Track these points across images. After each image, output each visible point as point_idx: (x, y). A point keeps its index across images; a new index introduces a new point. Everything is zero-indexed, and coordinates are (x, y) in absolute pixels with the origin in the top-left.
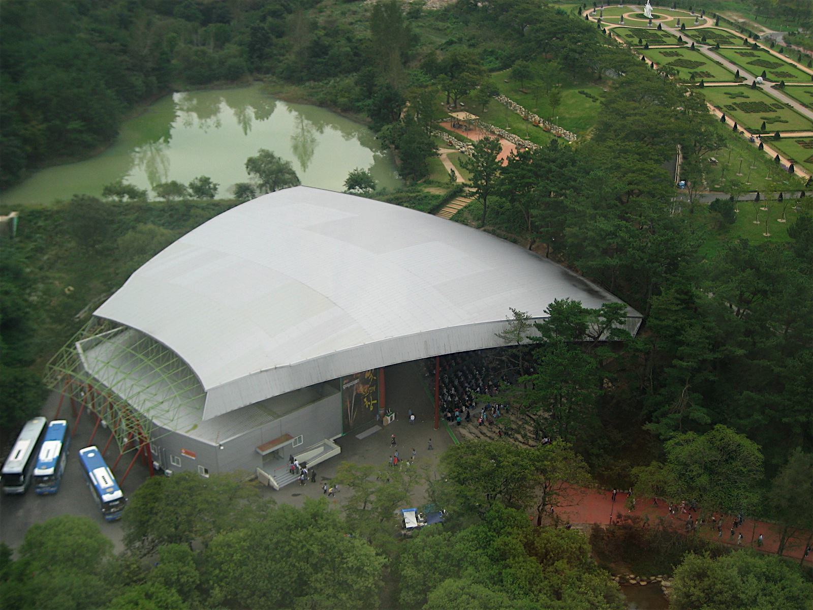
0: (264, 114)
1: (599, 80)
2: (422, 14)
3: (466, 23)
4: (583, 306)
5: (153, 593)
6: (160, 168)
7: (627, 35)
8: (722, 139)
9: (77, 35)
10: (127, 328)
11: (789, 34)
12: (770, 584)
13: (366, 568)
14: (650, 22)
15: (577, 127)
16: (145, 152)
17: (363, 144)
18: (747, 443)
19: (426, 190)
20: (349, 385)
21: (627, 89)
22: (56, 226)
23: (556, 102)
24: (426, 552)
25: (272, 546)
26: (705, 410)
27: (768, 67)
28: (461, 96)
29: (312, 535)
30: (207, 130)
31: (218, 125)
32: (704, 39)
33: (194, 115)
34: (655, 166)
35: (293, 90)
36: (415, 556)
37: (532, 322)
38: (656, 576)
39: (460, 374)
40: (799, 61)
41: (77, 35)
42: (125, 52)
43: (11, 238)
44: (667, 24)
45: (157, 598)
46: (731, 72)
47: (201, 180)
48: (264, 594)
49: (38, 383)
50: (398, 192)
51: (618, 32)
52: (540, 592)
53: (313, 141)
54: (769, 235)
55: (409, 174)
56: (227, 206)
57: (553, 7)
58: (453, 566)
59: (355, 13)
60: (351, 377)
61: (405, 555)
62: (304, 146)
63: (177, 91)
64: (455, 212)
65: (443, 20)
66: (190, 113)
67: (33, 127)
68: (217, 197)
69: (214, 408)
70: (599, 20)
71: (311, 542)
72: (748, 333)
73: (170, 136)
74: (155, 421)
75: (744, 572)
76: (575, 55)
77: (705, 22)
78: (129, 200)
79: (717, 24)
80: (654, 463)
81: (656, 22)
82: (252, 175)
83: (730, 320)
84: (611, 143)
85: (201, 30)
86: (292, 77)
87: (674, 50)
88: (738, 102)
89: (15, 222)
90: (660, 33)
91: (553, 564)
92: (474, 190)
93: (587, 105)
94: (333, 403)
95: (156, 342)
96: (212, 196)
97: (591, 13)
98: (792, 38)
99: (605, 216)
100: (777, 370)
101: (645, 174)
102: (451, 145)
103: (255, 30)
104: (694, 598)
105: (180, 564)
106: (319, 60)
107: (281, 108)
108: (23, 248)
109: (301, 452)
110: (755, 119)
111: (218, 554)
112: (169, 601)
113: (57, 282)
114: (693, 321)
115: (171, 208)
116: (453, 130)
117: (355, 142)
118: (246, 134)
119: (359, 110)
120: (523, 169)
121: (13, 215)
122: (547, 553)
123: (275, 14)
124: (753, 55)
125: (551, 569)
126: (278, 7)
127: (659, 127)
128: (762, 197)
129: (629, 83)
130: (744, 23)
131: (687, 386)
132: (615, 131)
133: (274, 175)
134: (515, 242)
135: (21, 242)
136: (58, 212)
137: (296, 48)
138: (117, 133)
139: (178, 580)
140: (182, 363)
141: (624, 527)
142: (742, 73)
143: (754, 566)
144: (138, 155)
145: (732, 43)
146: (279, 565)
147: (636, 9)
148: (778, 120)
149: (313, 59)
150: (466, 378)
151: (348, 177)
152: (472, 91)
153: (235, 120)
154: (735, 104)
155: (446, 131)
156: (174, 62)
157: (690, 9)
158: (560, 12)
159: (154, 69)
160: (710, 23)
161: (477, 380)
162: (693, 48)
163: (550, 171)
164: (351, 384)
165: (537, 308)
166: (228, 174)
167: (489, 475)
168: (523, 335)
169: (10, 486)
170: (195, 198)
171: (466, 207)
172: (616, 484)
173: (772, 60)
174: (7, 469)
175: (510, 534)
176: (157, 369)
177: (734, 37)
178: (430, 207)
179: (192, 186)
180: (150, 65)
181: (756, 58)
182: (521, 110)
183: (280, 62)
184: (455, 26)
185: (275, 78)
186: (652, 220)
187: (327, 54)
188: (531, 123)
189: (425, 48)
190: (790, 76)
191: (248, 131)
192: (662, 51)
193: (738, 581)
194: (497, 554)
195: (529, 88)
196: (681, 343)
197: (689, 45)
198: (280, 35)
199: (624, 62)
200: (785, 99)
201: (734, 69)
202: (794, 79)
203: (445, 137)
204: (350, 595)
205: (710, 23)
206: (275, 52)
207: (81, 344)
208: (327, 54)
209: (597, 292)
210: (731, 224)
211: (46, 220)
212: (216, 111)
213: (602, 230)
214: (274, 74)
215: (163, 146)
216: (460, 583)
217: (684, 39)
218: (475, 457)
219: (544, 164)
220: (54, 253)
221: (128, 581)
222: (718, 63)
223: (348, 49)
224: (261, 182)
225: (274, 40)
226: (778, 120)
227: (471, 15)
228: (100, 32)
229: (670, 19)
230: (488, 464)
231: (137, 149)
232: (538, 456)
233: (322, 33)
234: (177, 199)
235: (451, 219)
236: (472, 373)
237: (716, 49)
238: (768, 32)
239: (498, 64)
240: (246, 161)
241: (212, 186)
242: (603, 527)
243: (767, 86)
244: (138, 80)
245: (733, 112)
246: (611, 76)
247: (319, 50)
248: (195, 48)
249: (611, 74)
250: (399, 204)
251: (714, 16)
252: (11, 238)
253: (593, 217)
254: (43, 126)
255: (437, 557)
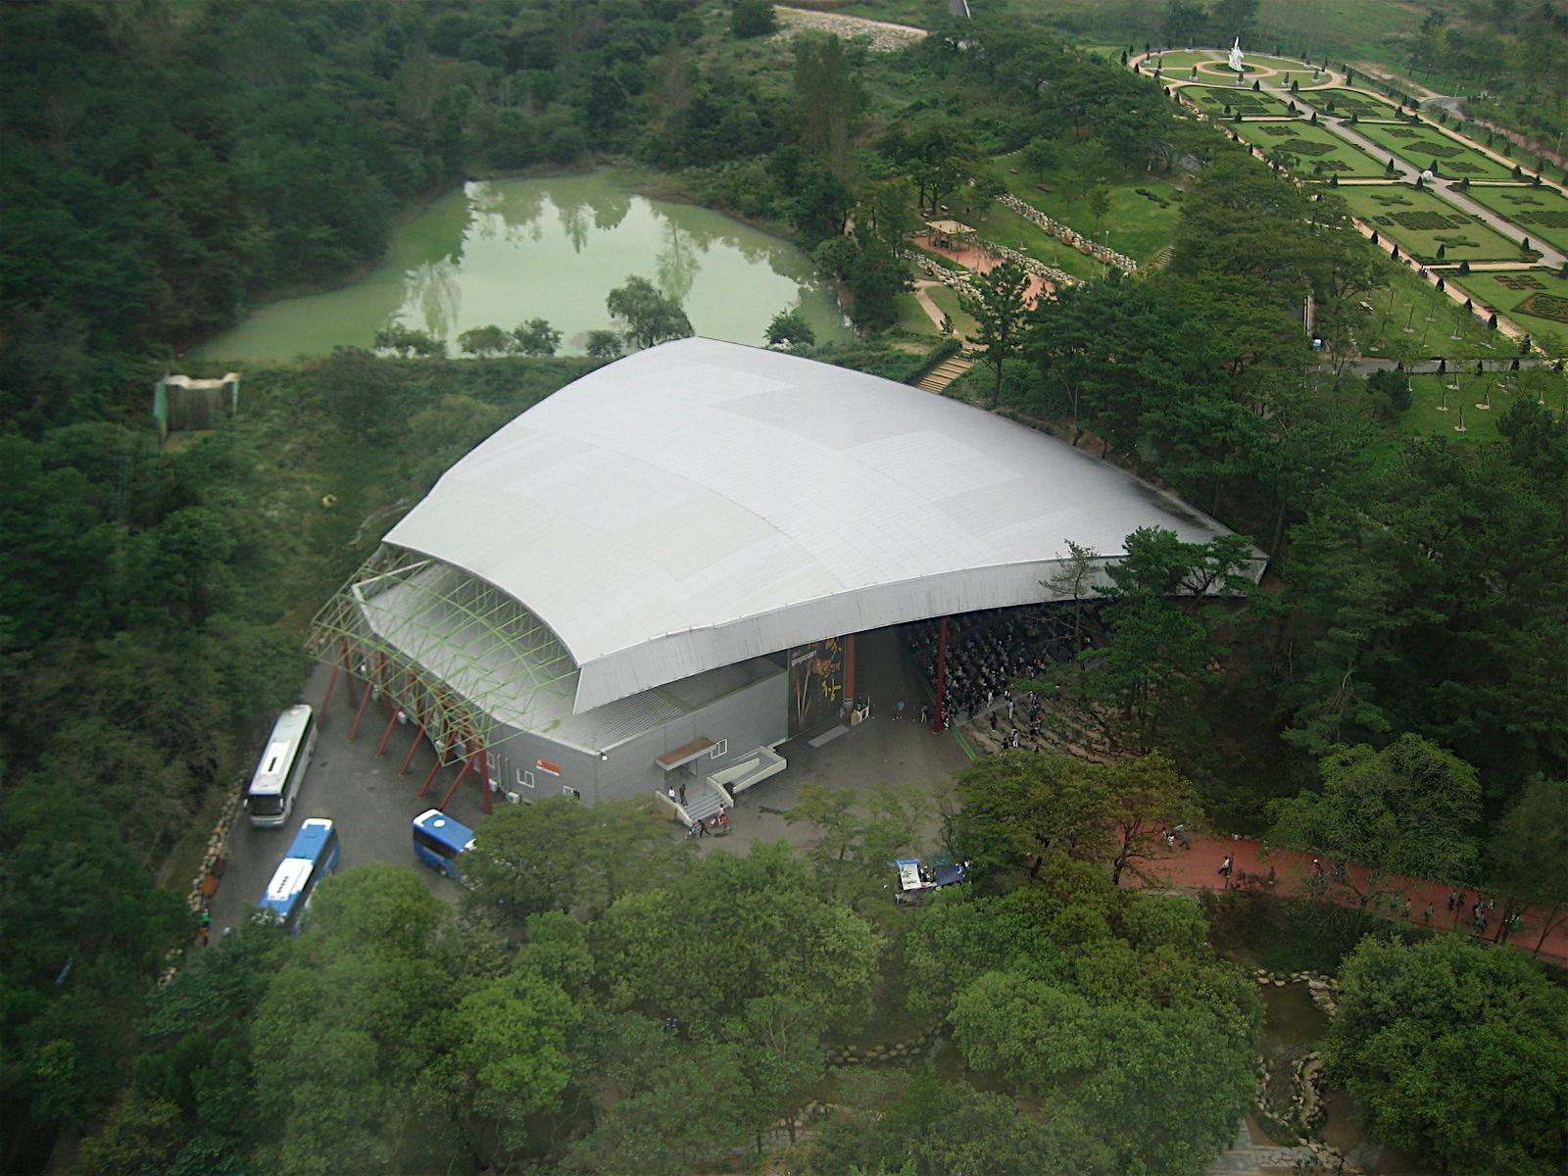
0: (609, 219)
1: (1168, 173)
2: (868, 59)
3: (942, 75)
4: (1181, 539)
5: (525, 990)
6: (446, 305)
7: (1204, 99)
8: (1384, 272)
9: (315, 86)
10: (437, 561)
11: (1469, 100)
12: (1500, 989)
13: (856, 954)
14: (1241, 78)
15: (1138, 248)
16: (422, 279)
17: (778, 270)
18: (1454, 763)
19: (898, 347)
20: (800, 660)
21: (1222, 189)
22: (302, 397)
23: (1101, 206)
24: (947, 929)
25: (708, 917)
26: (1379, 709)
27: (1440, 155)
28: (940, 196)
29: (769, 900)
30: (519, 244)
31: (537, 235)
32: (1331, 107)
33: (499, 219)
34: (1282, 314)
35: (661, 179)
36: (931, 936)
37: (1102, 563)
38: (1300, 972)
39: (970, 645)
40: (1489, 144)
41: (315, 86)
42: (391, 114)
43: (230, 415)
44: (1267, 80)
45: (533, 998)
46: (1379, 162)
47: (534, 325)
48: (698, 994)
49: (297, 649)
50: (852, 349)
51: (1190, 94)
52: (1136, 995)
53: (692, 264)
54: (1463, 429)
55: (869, 320)
56: (574, 371)
57: (1083, 51)
58: (992, 951)
59: (757, 55)
60: (803, 649)
61: (914, 934)
62: (677, 271)
63: (473, 180)
64: (947, 382)
65: (903, 70)
66: (492, 215)
67: (254, 235)
68: (559, 354)
69: (592, 694)
70: (1157, 74)
71: (769, 912)
72: (1450, 588)
73: (461, 253)
74: (496, 715)
75: (1460, 969)
76: (1130, 134)
77: (1329, 78)
78: (418, 357)
79: (1349, 83)
80: (1304, 792)
81: (1251, 78)
82: (618, 317)
83: (1421, 565)
84: (1205, 276)
85: (508, 80)
86: (661, 158)
87: (1283, 125)
88: (1395, 212)
89: (236, 390)
90: (1257, 96)
91: (1151, 951)
92: (983, 348)
93: (1153, 213)
94: (775, 689)
95: (489, 586)
96: (551, 351)
97: (1142, 62)
98: (1474, 106)
99: (1206, 394)
100: (1498, 647)
101: (1266, 327)
102: (930, 274)
103: (599, 82)
104: (1378, 1008)
105: (565, 944)
106: (705, 132)
107: (639, 208)
108: (248, 432)
109: (725, 767)
110: (1426, 241)
111: (620, 927)
112: (553, 1001)
113: (308, 488)
114: (1360, 566)
115: (491, 370)
116: (932, 249)
117: (764, 265)
118: (578, 250)
119: (775, 215)
120: (1067, 316)
121: (230, 377)
122: (1143, 931)
123: (627, 55)
124: (1413, 135)
125: (1149, 957)
126: (632, 43)
127: (1283, 252)
128: (1449, 366)
129: (1222, 179)
130: (1392, 80)
131: (1350, 671)
132: (1210, 256)
133: (652, 318)
134: (1049, 432)
135: (245, 422)
136: (303, 374)
137: (667, 112)
138: (385, 247)
139: (562, 968)
140: (533, 620)
141: (1250, 894)
142: (1398, 165)
143: (1475, 959)
144: (413, 282)
145: (1377, 115)
146: (720, 948)
147: (1214, 56)
148: (1462, 242)
149: (696, 130)
150: (981, 651)
151: (770, 323)
152: (963, 186)
153: (561, 227)
154: (1390, 214)
155: (921, 251)
156: (465, 131)
157: (1303, 57)
158: (1096, 60)
159: (438, 143)
160: (1337, 80)
161: (999, 654)
162: (1314, 122)
163: (1112, 319)
164: (803, 658)
165: (1109, 542)
166: (579, 313)
167: (1043, 807)
168: (1083, 583)
169: (260, 815)
170: (524, 354)
171: (964, 376)
172: (1246, 824)
173: (1445, 143)
174: (256, 788)
175: (1084, 902)
176: (495, 631)
177: (1380, 104)
178: (905, 374)
179: (519, 334)
180: (433, 136)
181: (1419, 140)
182: (1045, 223)
183: (639, 134)
184: (922, 80)
185: (631, 161)
186: (1286, 402)
187: (718, 123)
188: (1059, 240)
189: (876, 115)
190: (1476, 170)
191: (582, 246)
192: (1265, 125)
193: (1452, 982)
194: (1065, 933)
195: (1056, 183)
196: (1344, 602)
197: (1308, 117)
198: (637, 90)
199: (1206, 145)
200: (1472, 209)
201: (1386, 158)
202: (1483, 175)
203: (922, 261)
204: (831, 996)
205: (1337, 80)
206: (631, 118)
207: (361, 589)
208: (718, 123)
209: (1191, 516)
210: (1402, 410)
211: (284, 386)
212: (534, 213)
213: (1204, 416)
214: (629, 153)
215: (450, 269)
216: (1010, 978)
217: (1298, 106)
218: (1020, 779)
219: (1101, 307)
220: (300, 440)
221: (478, 969)
222: (1356, 147)
223: (754, 114)
224: (629, 329)
225: (630, 98)
226: (1462, 242)
227: (950, 61)
228: (351, 81)
229: (1272, 72)
230: (1040, 792)
231: (410, 273)
232: (1121, 780)
233: (706, 87)
234: (496, 354)
235: (942, 394)
236: (986, 639)
237: (1351, 123)
238: (1433, 96)
239: (998, 143)
240: (607, 295)
241: (550, 334)
242: (1216, 893)
243: (1440, 186)
244: (413, 161)
245: (1387, 228)
246: (1190, 167)
247: (704, 115)
248: (501, 110)
249: (1189, 163)
250: (857, 368)
251: (1344, 69)
252: (230, 415)
253: (1188, 397)
254: (270, 234)
255: (966, 938)
